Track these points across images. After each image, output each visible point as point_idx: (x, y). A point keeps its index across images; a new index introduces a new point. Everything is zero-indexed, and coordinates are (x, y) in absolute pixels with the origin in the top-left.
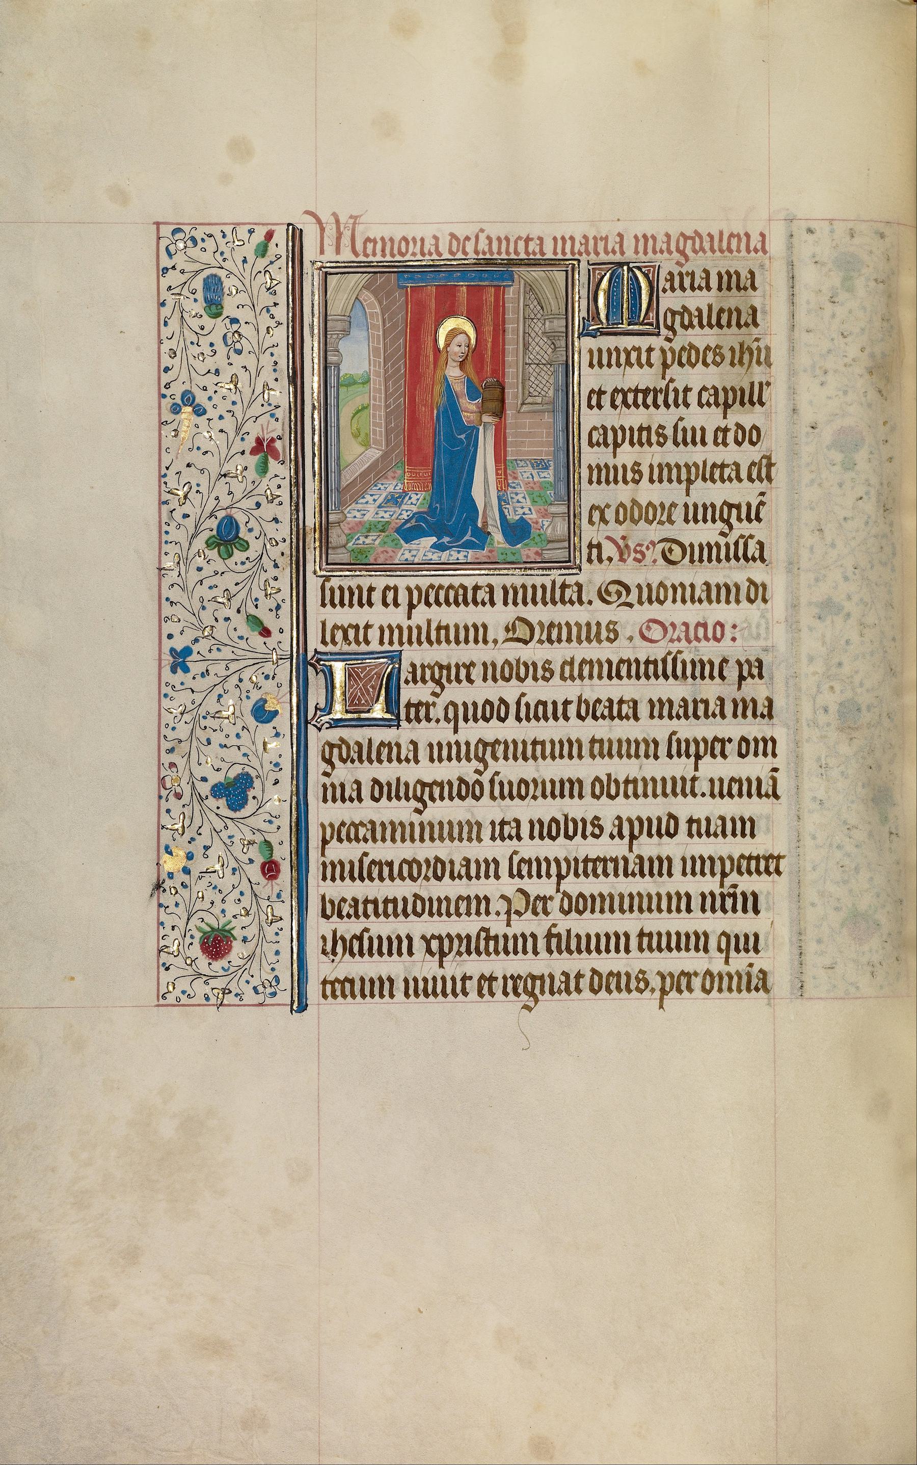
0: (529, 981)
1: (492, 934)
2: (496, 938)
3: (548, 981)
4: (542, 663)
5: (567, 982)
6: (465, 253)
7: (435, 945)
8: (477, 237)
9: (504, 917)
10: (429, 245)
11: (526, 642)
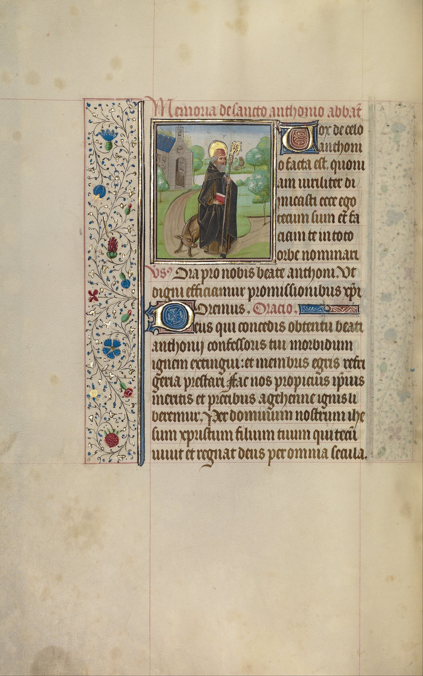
0: (346, 200)
1: (211, 430)
2: (213, 432)
3: (218, 453)
4: (207, 324)
5: (227, 454)
6: (228, 115)
7: (186, 435)
8: (234, 106)
10: (210, 111)
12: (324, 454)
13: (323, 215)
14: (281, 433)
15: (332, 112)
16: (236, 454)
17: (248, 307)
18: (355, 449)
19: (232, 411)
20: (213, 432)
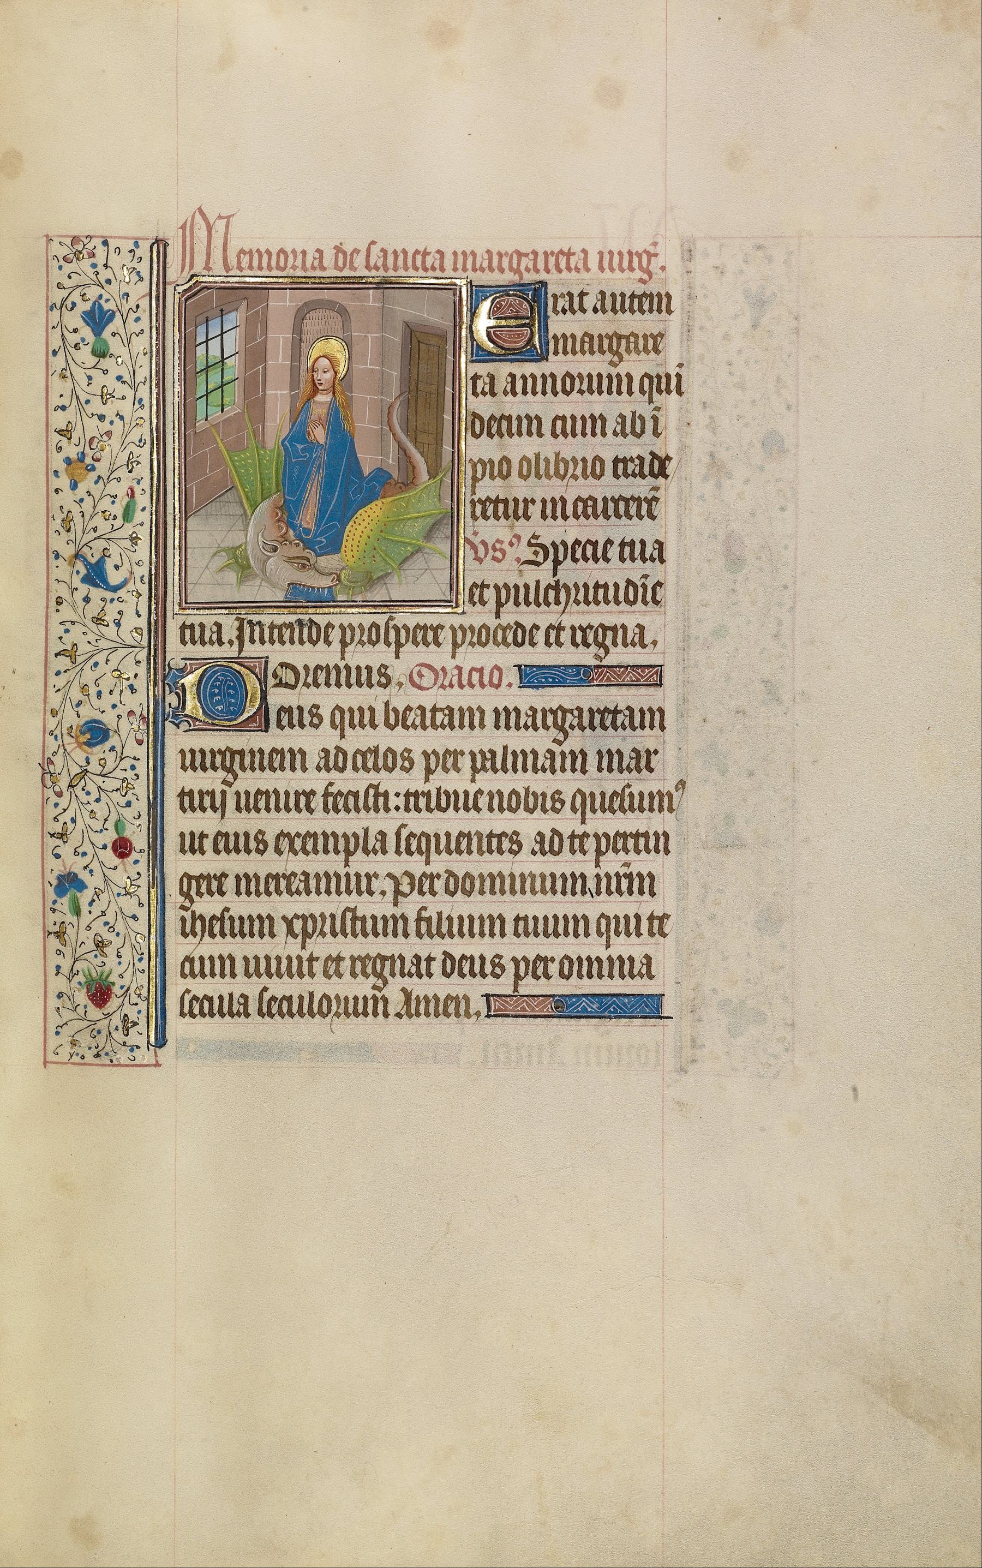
1: (359, 914)
2: (363, 919)
6: (353, 268)
7: (298, 926)
8: (368, 250)
9: (390, 896)
11: (293, 687)
12: (645, 967)
13: (548, 500)
14: (521, 923)
15: (542, 843)
16: (436, 967)
17: (399, 670)
18: (231, 995)
19: (450, 874)
20: (363, 919)
